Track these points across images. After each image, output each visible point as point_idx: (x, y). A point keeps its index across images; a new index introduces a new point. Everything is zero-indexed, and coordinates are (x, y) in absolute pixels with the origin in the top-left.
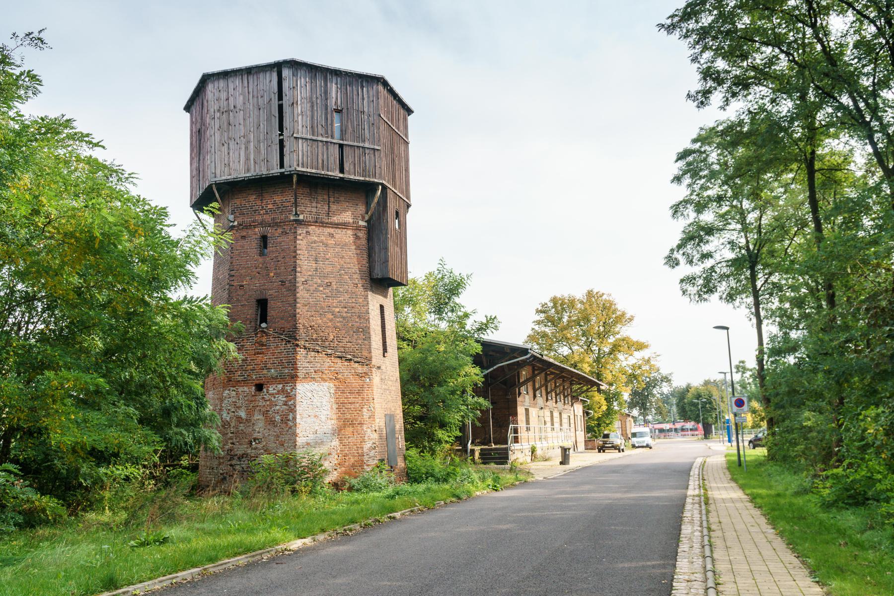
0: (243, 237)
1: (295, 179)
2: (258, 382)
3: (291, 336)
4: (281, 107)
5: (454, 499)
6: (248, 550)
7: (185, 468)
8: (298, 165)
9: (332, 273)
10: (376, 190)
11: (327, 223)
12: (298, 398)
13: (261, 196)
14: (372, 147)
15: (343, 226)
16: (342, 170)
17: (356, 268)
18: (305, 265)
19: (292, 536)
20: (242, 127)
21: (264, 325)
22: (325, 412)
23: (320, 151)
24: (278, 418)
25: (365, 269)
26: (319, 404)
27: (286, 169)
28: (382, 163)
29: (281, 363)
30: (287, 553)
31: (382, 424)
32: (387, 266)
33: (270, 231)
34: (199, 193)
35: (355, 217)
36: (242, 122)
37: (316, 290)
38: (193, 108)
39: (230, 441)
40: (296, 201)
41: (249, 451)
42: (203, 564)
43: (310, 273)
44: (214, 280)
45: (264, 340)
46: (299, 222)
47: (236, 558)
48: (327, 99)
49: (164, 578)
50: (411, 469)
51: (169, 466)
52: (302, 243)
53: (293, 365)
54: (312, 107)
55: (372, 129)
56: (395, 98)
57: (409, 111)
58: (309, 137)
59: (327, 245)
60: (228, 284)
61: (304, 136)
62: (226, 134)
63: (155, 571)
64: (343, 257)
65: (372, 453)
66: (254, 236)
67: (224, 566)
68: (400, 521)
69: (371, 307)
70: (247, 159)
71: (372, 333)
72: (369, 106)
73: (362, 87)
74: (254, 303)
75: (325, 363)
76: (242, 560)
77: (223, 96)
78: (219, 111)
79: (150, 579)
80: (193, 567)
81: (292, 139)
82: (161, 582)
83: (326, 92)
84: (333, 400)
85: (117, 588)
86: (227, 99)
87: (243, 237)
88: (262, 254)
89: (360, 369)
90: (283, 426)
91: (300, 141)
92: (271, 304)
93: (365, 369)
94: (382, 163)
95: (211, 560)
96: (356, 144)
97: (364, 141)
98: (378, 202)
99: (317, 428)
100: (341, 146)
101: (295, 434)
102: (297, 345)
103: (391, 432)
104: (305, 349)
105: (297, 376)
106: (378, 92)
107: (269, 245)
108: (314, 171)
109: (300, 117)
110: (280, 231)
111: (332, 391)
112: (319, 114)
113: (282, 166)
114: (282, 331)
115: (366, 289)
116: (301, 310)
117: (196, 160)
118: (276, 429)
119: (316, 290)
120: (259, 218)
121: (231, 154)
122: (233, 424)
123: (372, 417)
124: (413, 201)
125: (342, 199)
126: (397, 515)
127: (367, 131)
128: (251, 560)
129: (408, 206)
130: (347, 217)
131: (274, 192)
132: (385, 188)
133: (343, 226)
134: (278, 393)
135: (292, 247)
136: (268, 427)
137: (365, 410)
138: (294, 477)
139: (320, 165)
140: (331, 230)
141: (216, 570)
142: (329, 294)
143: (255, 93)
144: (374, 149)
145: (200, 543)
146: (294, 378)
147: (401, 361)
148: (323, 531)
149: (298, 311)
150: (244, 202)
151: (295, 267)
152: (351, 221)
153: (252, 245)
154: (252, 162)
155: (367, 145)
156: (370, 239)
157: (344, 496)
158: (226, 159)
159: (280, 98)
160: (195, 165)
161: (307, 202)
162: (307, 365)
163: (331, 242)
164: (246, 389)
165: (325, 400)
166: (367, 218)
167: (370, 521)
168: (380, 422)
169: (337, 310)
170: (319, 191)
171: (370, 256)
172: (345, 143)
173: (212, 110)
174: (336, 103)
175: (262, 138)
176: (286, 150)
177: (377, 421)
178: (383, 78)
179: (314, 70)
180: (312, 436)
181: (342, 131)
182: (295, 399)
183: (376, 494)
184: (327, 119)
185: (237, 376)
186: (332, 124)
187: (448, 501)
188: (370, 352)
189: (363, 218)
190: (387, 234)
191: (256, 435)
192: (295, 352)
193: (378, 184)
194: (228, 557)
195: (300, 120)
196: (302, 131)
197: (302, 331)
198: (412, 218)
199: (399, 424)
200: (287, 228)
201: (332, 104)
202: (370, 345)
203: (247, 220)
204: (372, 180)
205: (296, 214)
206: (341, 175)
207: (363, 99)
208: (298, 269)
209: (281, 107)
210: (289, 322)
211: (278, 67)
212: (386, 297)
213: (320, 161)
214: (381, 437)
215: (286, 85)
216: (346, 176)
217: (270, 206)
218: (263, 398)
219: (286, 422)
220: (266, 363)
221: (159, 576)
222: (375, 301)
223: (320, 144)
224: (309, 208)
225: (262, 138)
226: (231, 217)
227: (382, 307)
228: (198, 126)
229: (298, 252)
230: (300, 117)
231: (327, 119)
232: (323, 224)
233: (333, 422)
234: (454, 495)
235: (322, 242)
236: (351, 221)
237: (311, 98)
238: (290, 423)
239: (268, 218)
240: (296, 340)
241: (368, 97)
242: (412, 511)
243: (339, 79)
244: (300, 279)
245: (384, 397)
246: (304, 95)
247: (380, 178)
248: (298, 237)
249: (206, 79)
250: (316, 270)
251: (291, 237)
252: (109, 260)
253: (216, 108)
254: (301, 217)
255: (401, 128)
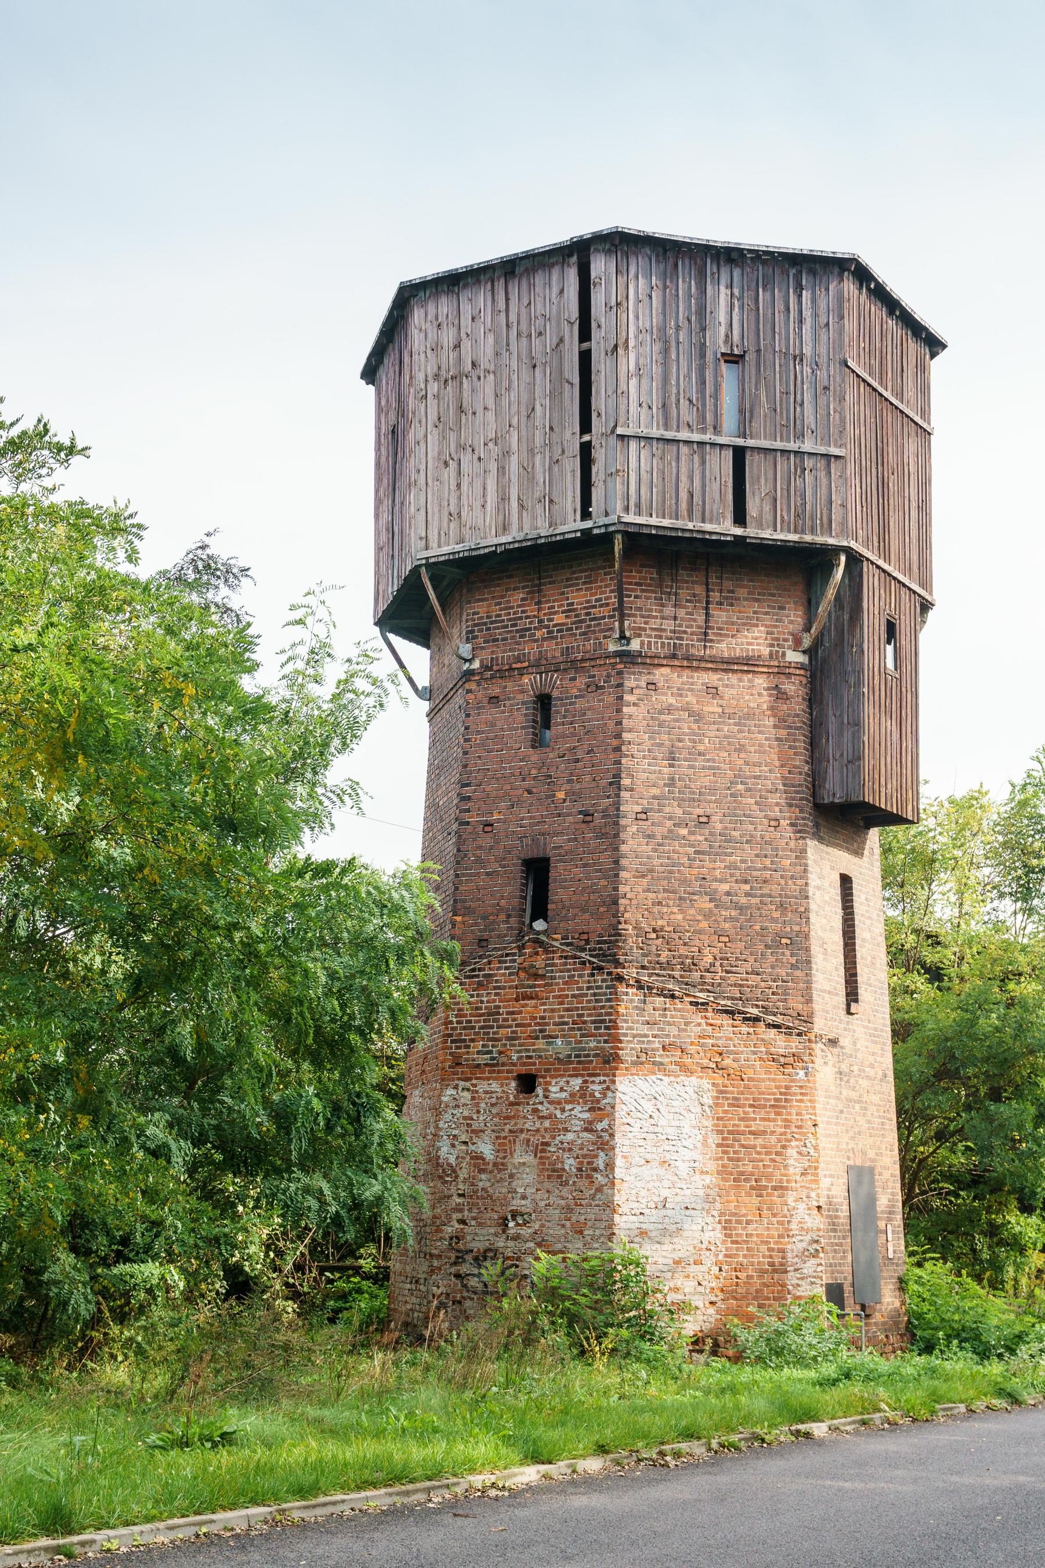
0: (494, 700)
1: (618, 547)
2: (523, 1070)
3: (604, 954)
4: (585, 358)
5: (996, 1402)
6: (397, 1477)
7: (366, 1277)
8: (627, 509)
9: (713, 790)
10: (829, 568)
11: (701, 659)
12: (620, 1112)
13: (536, 593)
14: (822, 450)
15: (746, 664)
16: (740, 517)
17: (774, 778)
18: (643, 770)
19: (516, 1457)
20: (491, 416)
21: (539, 925)
22: (688, 1155)
23: (684, 470)
24: (570, 1163)
25: (799, 779)
26: (672, 1132)
27: (597, 522)
28: (849, 492)
29: (579, 1023)
30: (493, 1493)
31: (839, 1193)
32: (858, 772)
33: (558, 684)
34: (392, 588)
35: (775, 642)
36: (490, 403)
37: (671, 836)
38: (382, 373)
39: (456, 1216)
40: (621, 602)
41: (500, 1243)
42: (277, 1499)
43: (655, 791)
44: (428, 808)
45: (540, 962)
46: (628, 658)
47: (363, 1494)
48: (704, 329)
49: (182, 1521)
50: (920, 1316)
51: (332, 1269)
52: (635, 714)
53: (608, 1026)
54: (666, 351)
55: (822, 401)
56: (891, 313)
57: (934, 344)
58: (655, 433)
59: (698, 717)
60: (458, 815)
61: (644, 431)
62: (452, 437)
63: (166, 1503)
64: (741, 749)
65: (809, 1267)
66: (520, 697)
67: (330, 1509)
68: (821, 1443)
69: (813, 880)
70: (503, 499)
71: (815, 949)
72: (816, 340)
73: (799, 288)
74: (516, 868)
75: (690, 1025)
76: (377, 1499)
77: (448, 337)
78: (437, 377)
79: (149, 1519)
80: (254, 1502)
81: (613, 440)
82: (171, 1528)
83: (702, 311)
84: (709, 1123)
85: (71, 1532)
86: (457, 346)
87: (494, 700)
88: (538, 742)
89: (781, 1043)
90: (582, 1184)
91: (633, 445)
92: (558, 871)
93: (795, 1044)
94: (849, 492)
95: (302, 1492)
96: (778, 445)
97: (800, 436)
98: (838, 598)
99: (665, 1193)
100: (739, 454)
101: (610, 1207)
102: (620, 979)
103: (863, 1216)
104: (640, 987)
105: (617, 1058)
106: (840, 299)
107: (556, 719)
108: (666, 522)
109: (633, 382)
110: (582, 681)
111: (708, 1100)
112: (683, 367)
113: (586, 515)
114: (581, 942)
115: (800, 832)
116: (632, 889)
117: (387, 503)
118: (565, 1192)
119: (671, 836)
120: (531, 650)
121: (464, 487)
122: (463, 1174)
123: (810, 1171)
124: (939, 594)
125: (742, 593)
126: (820, 1430)
127: (808, 408)
128: (399, 1500)
129: (925, 606)
130: (754, 641)
131: (569, 582)
132: (855, 560)
133: (746, 664)
134: (572, 1098)
135: (611, 724)
136: (547, 1185)
137: (792, 1152)
138: (600, 1311)
139: (684, 506)
140: (713, 678)
141: (308, 1515)
142: (705, 846)
143: (524, 327)
144: (827, 457)
145: (301, 1451)
146: (610, 1061)
147: (901, 1031)
148: (602, 1449)
149: (622, 889)
150: (495, 610)
151: (617, 776)
152: (766, 651)
153: (514, 719)
154: (514, 504)
155: (808, 446)
156: (814, 699)
157: (712, 1372)
158: (453, 501)
159: (585, 334)
160: (385, 517)
161: (651, 604)
162: (645, 1030)
163: (712, 708)
164: (495, 1086)
165: (688, 1123)
166: (807, 642)
167: (734, 1438)
168: (832, 1185)
169: (725, 887)
170: (683, 574)
171: (814, 744)
172: (750, 442)
173: (420, 376)
174: (728, 338)
175: (538, 440)
176: (598, 471)
177: (825, 1183)
178: (854, 260)
179: (668, 252)
180: (654, 1215)
181: (741, 411)
182: (611, 1116)
183: (798, 1373)
184: (703, 382)
185: (475, 1053)
186: (716, 396)
187: (979, 1405)
188: (809, 1001)
189: (798, 642)
190: (859, 684)
191: (517, 1203)
192: (614, 997)
193: (837, 550)
194: (344, 1488)
195: (631, 390)
196: (640, 421)
197: (631, 942)
198: (933, 640)
199: (889, 1193)
200: (600, 674)
201: (717, 342)
202: (809, 983)
203: (504, 655)
204: (820, 539)
205: (623, 637)
206: (739, 531)
207: (801, 321)
208: (626, 782)
209: (585, 358)
210: (600, 918)
211: (579, 252)
212: (858, 852)
213: (684, 496)
214: (833, 1227)
215: (598, 299)
216: (750, 531)
217: (559, 619)
218: (536, 1111)
219: (587, 1175)
220: (543, 1022)
221: (172, 1516)
222: (825, 862)
223: (684, 449)
224: (656, 620)
225: (538, 440)
226: (465, 650)
227: (846, 881)
228: (392, 420)
229: (626, 736)
230: (633, 382)
231: (703, 382)
232: (691, 662)
233: (708, 1179)
234: (1001, 1392)
235: (686, 708)
236: (766, 651)
237: (662, 329)
238: (600, 1178)
239: (553, 650)
240: (617, 964)
241: (816, 315)
242: (864, 1423)
243: (737, 272)
244: (630, 807)
245: (849, 1117)
246: (644, 323)
247: (844, 532)
248: (627, 697)
249: (408, 297)
250: (671, 782)
251: (610, 699)
252: (162, 763)
253: (431, 369)
254: (635, 645)
255: (910, 392)
